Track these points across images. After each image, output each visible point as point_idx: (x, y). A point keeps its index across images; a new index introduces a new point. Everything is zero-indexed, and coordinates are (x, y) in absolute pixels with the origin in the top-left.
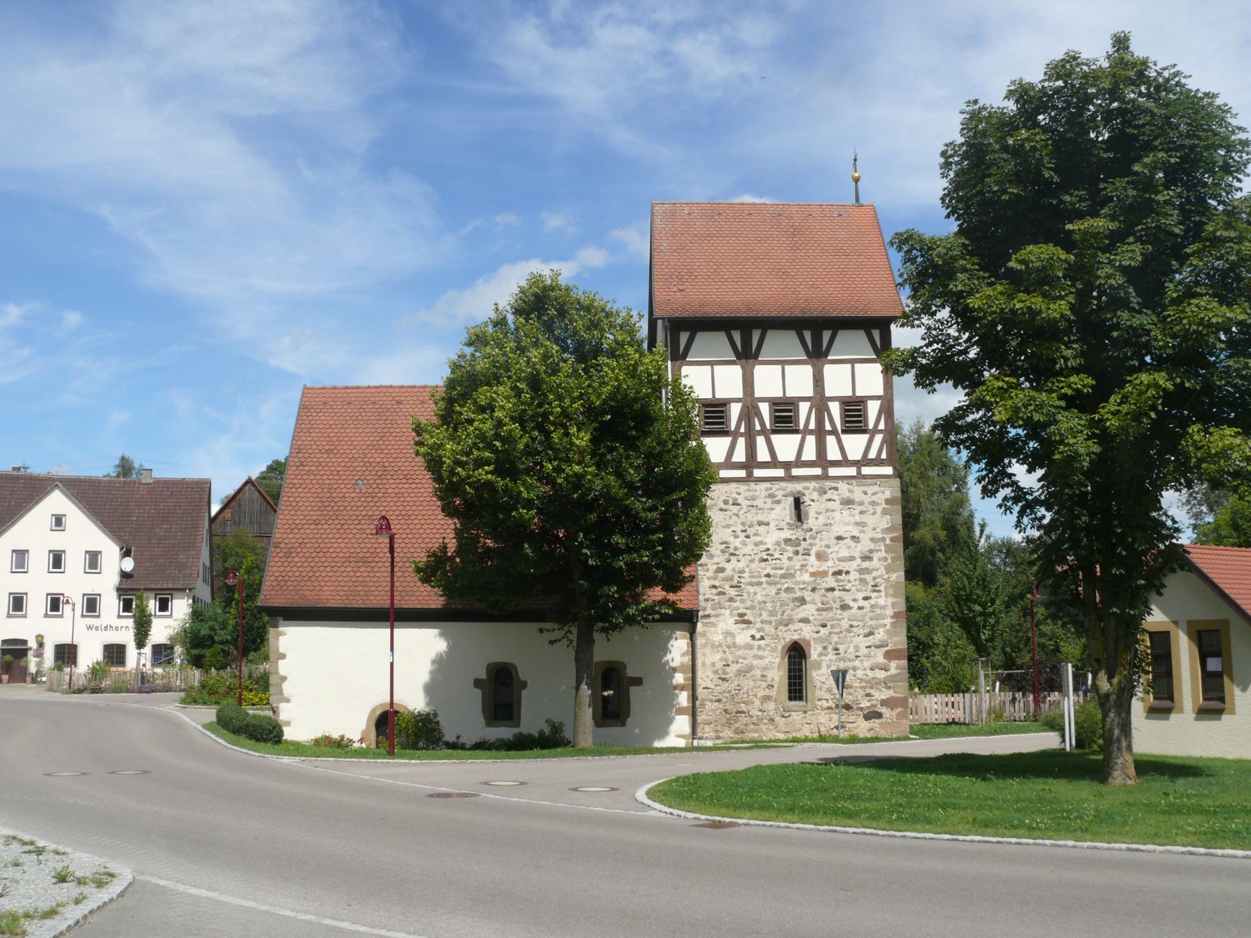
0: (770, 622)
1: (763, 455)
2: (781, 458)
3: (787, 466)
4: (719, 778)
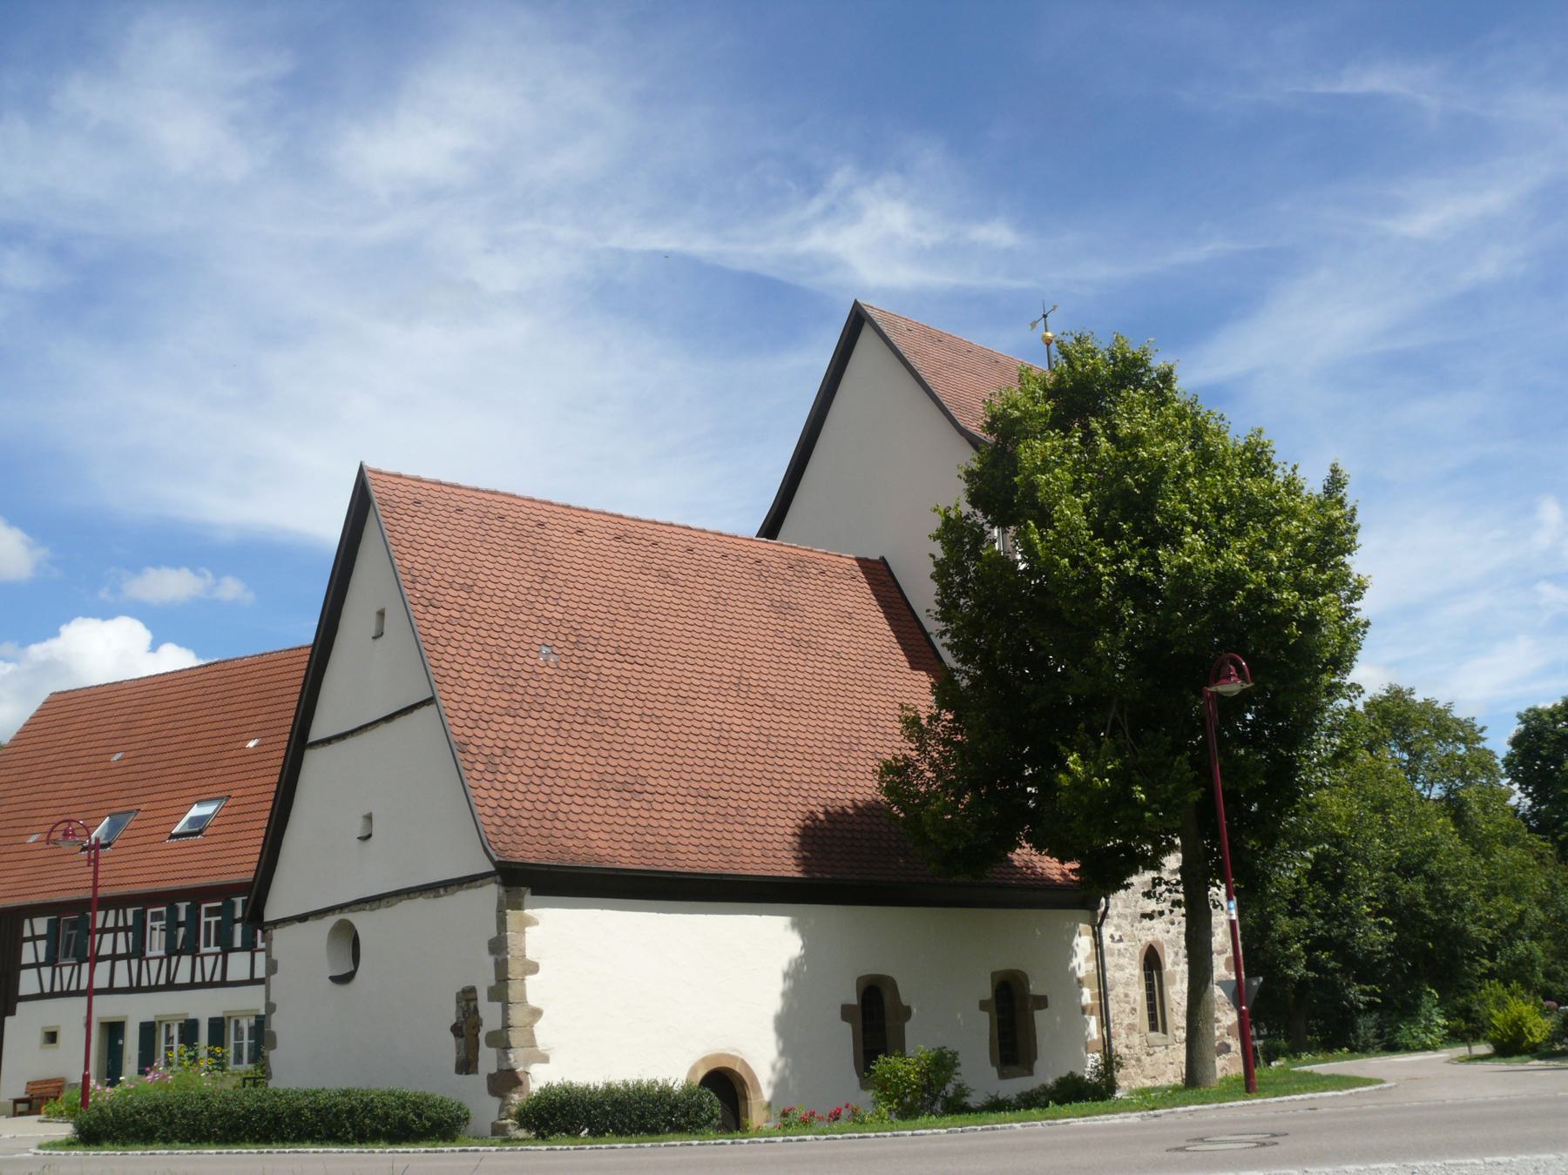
0: (1126, 917)
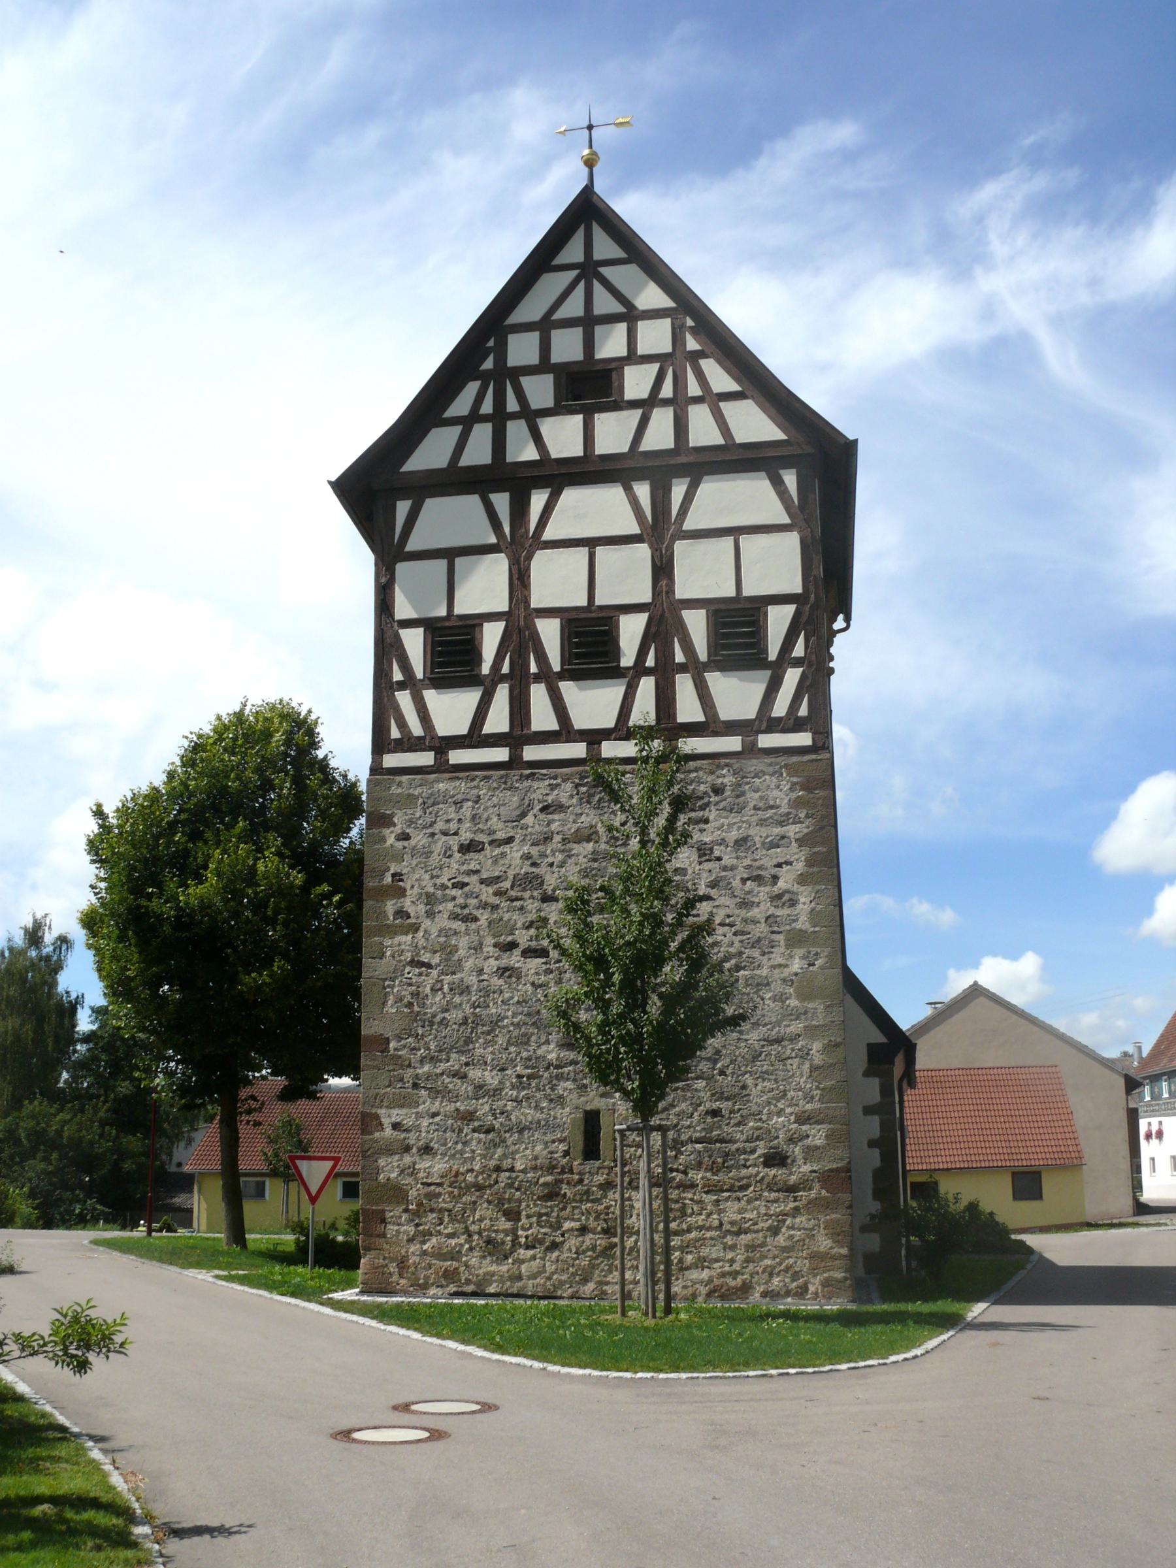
1: (542, 717)
2: (580, 721)
3: (594, 737)
4: (105, 1240)
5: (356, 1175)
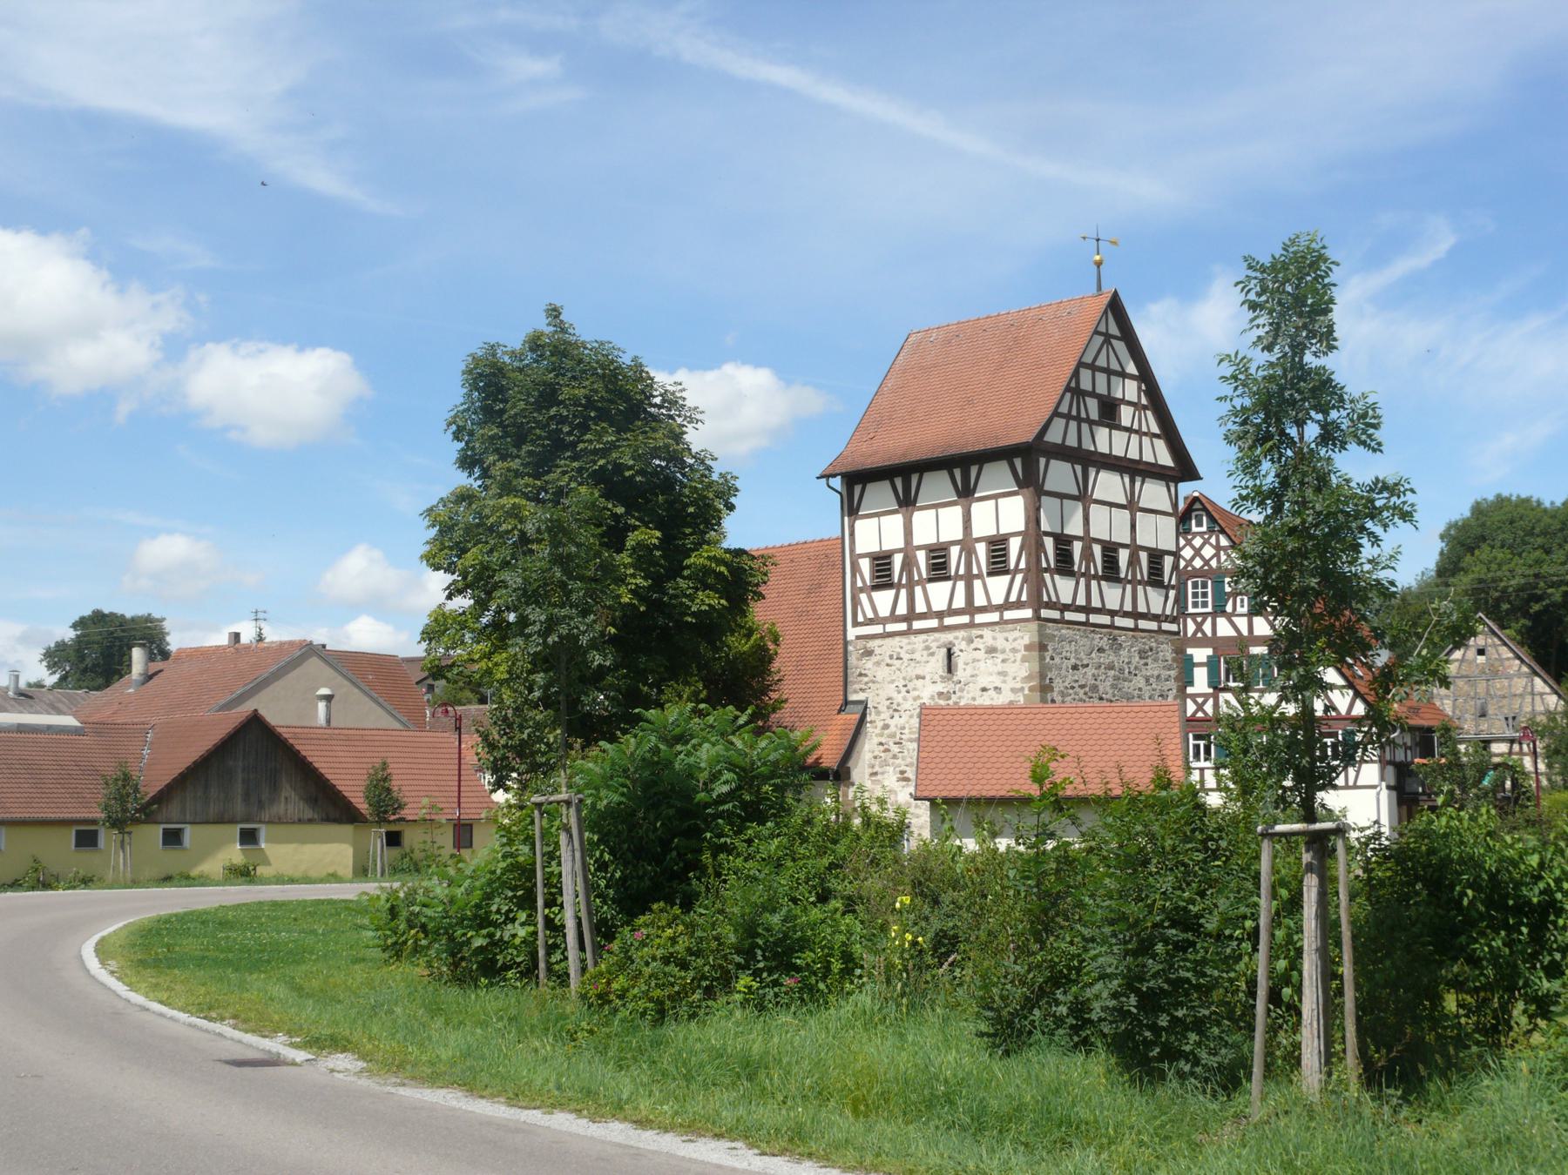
5: (94, 822)
